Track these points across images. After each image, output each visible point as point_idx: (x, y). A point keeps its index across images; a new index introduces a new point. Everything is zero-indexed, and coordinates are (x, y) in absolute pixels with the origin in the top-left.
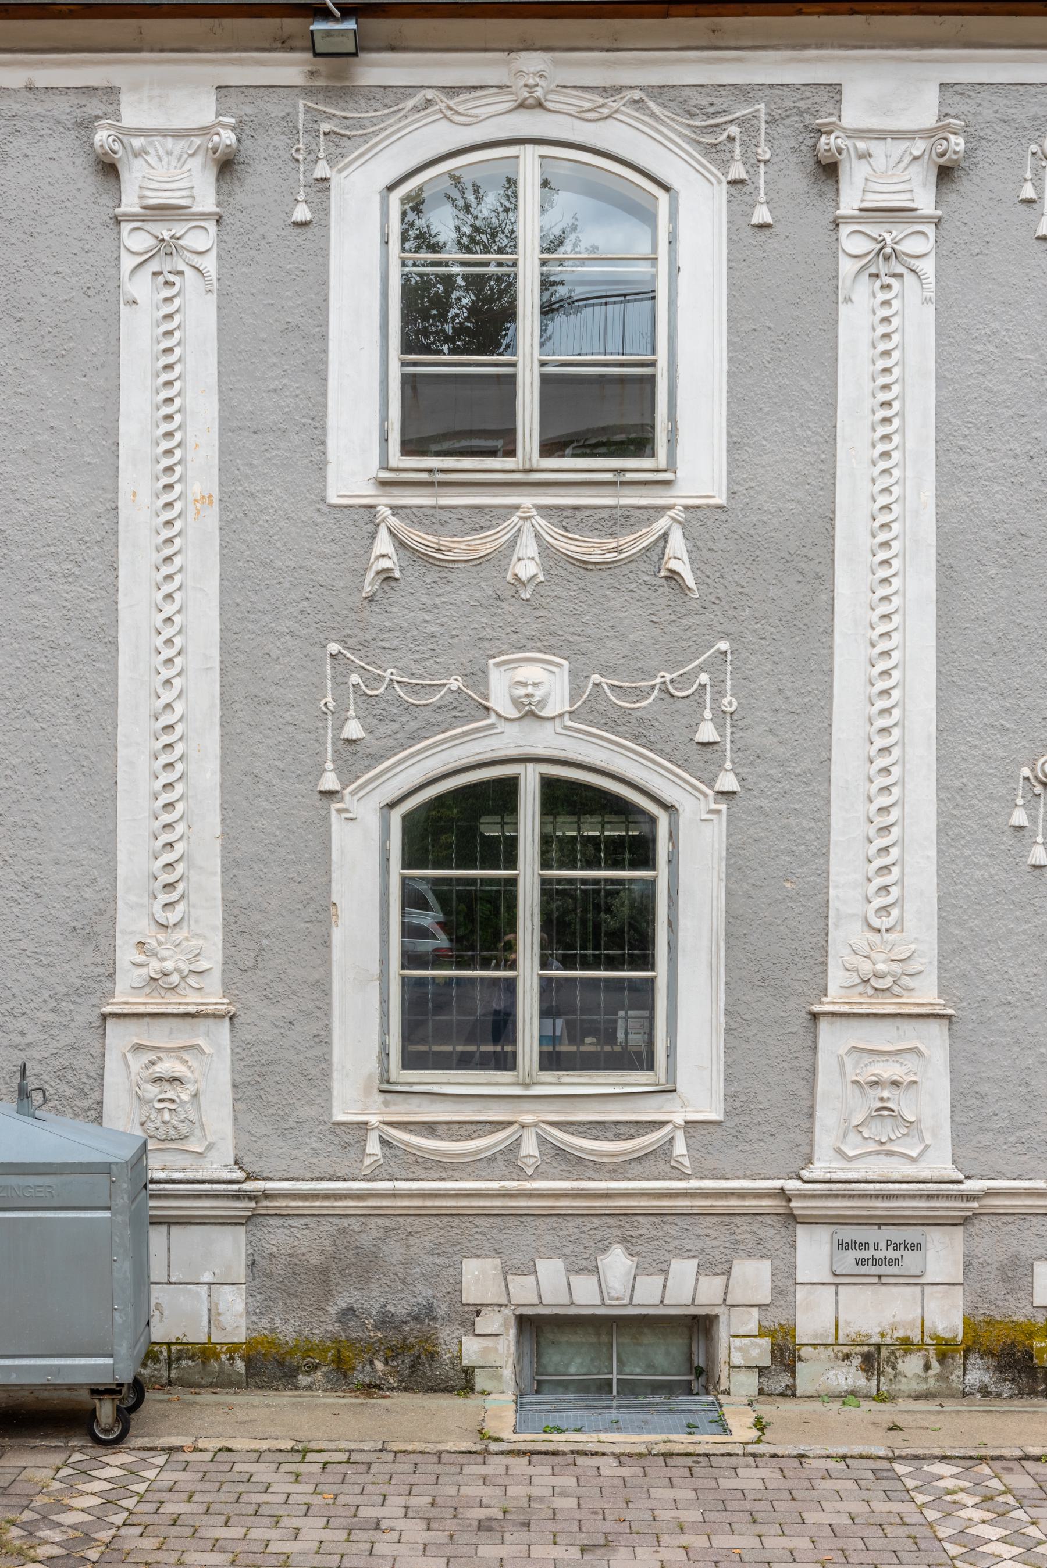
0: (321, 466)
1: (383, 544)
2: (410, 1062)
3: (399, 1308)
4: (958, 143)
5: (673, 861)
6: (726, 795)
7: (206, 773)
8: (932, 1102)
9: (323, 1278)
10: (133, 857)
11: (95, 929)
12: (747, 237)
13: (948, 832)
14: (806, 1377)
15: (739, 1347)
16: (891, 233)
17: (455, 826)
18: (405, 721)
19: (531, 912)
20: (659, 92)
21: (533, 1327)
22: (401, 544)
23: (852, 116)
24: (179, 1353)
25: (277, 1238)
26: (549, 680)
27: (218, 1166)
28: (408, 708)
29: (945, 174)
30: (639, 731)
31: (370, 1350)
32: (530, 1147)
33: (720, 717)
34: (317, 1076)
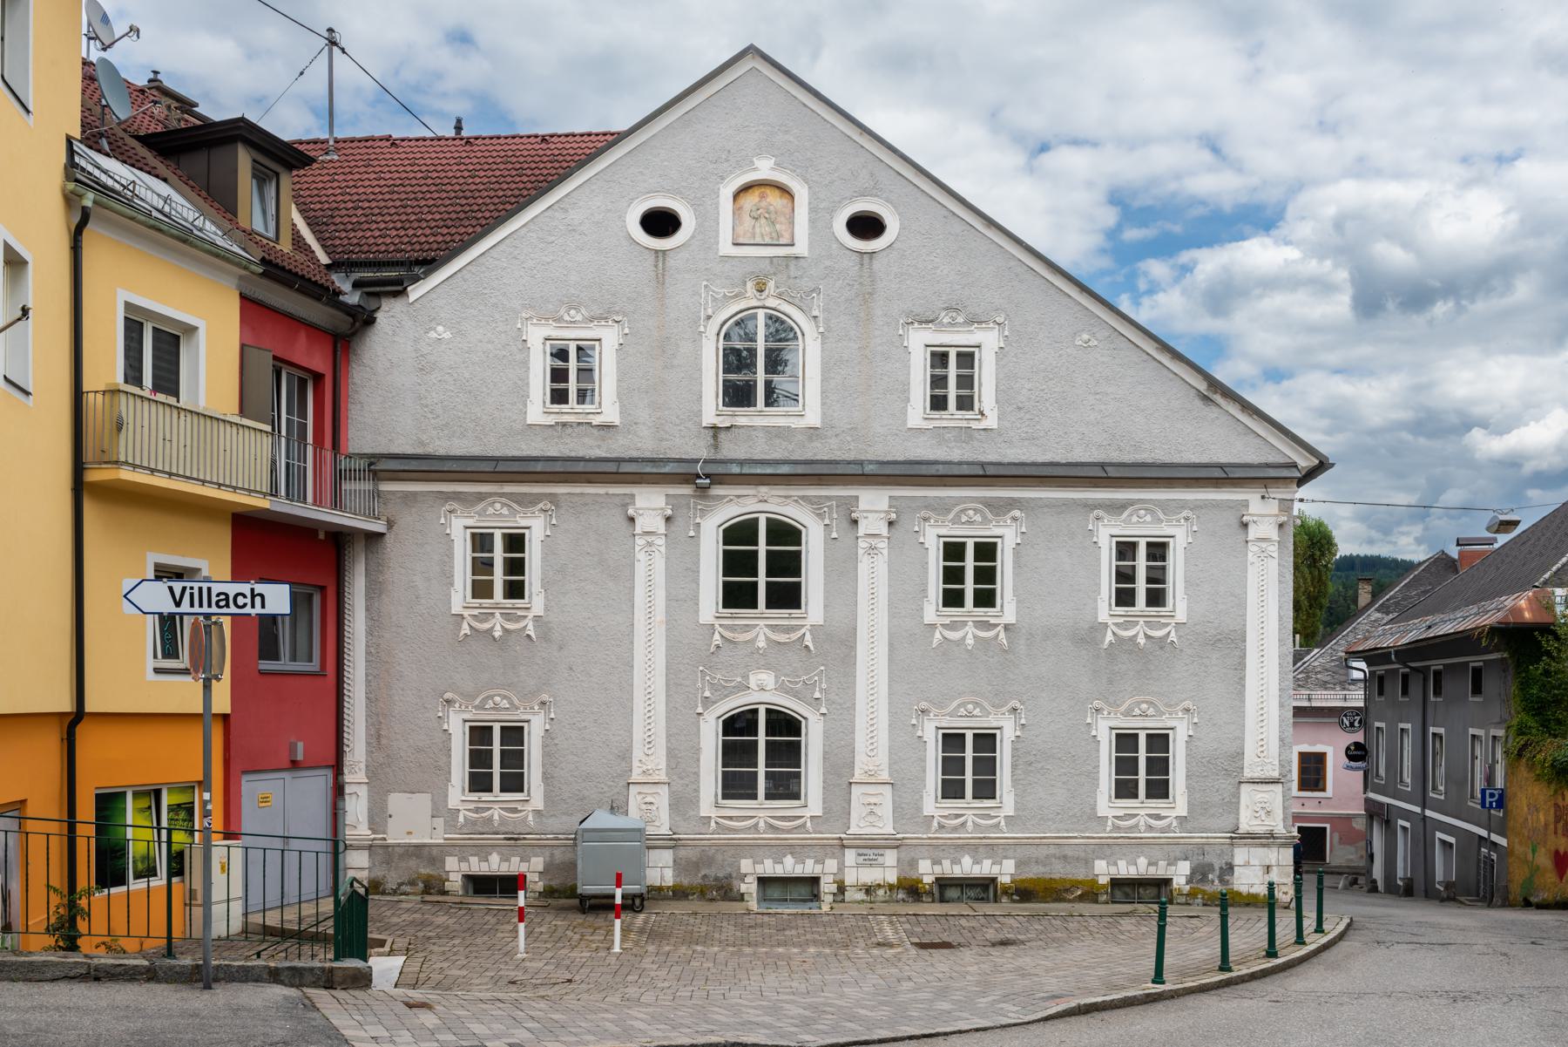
0: (697, 612)
1: (717, 636)
2: (725, 797)
3: (721, 875)
8: (886, 810)
9: (696, 865)
10: (638, 734)
11: (625, 756)
12: (830, 541)
14: (848, 895)
15: (827, 887)
16: (873, 541)
18: (723, 691)
19: (761, 748)
20: (802, 498)
21: (763, 881)
23: (862, 505)
24: (651, 889)
25: (682, 853)
26: (767, 678)
27: (665, 830)
29: (891, 523)
30: (796, 695)
31: (712, 888)
32: (762, 824)
33: (821, 690)
34: (695, 802)
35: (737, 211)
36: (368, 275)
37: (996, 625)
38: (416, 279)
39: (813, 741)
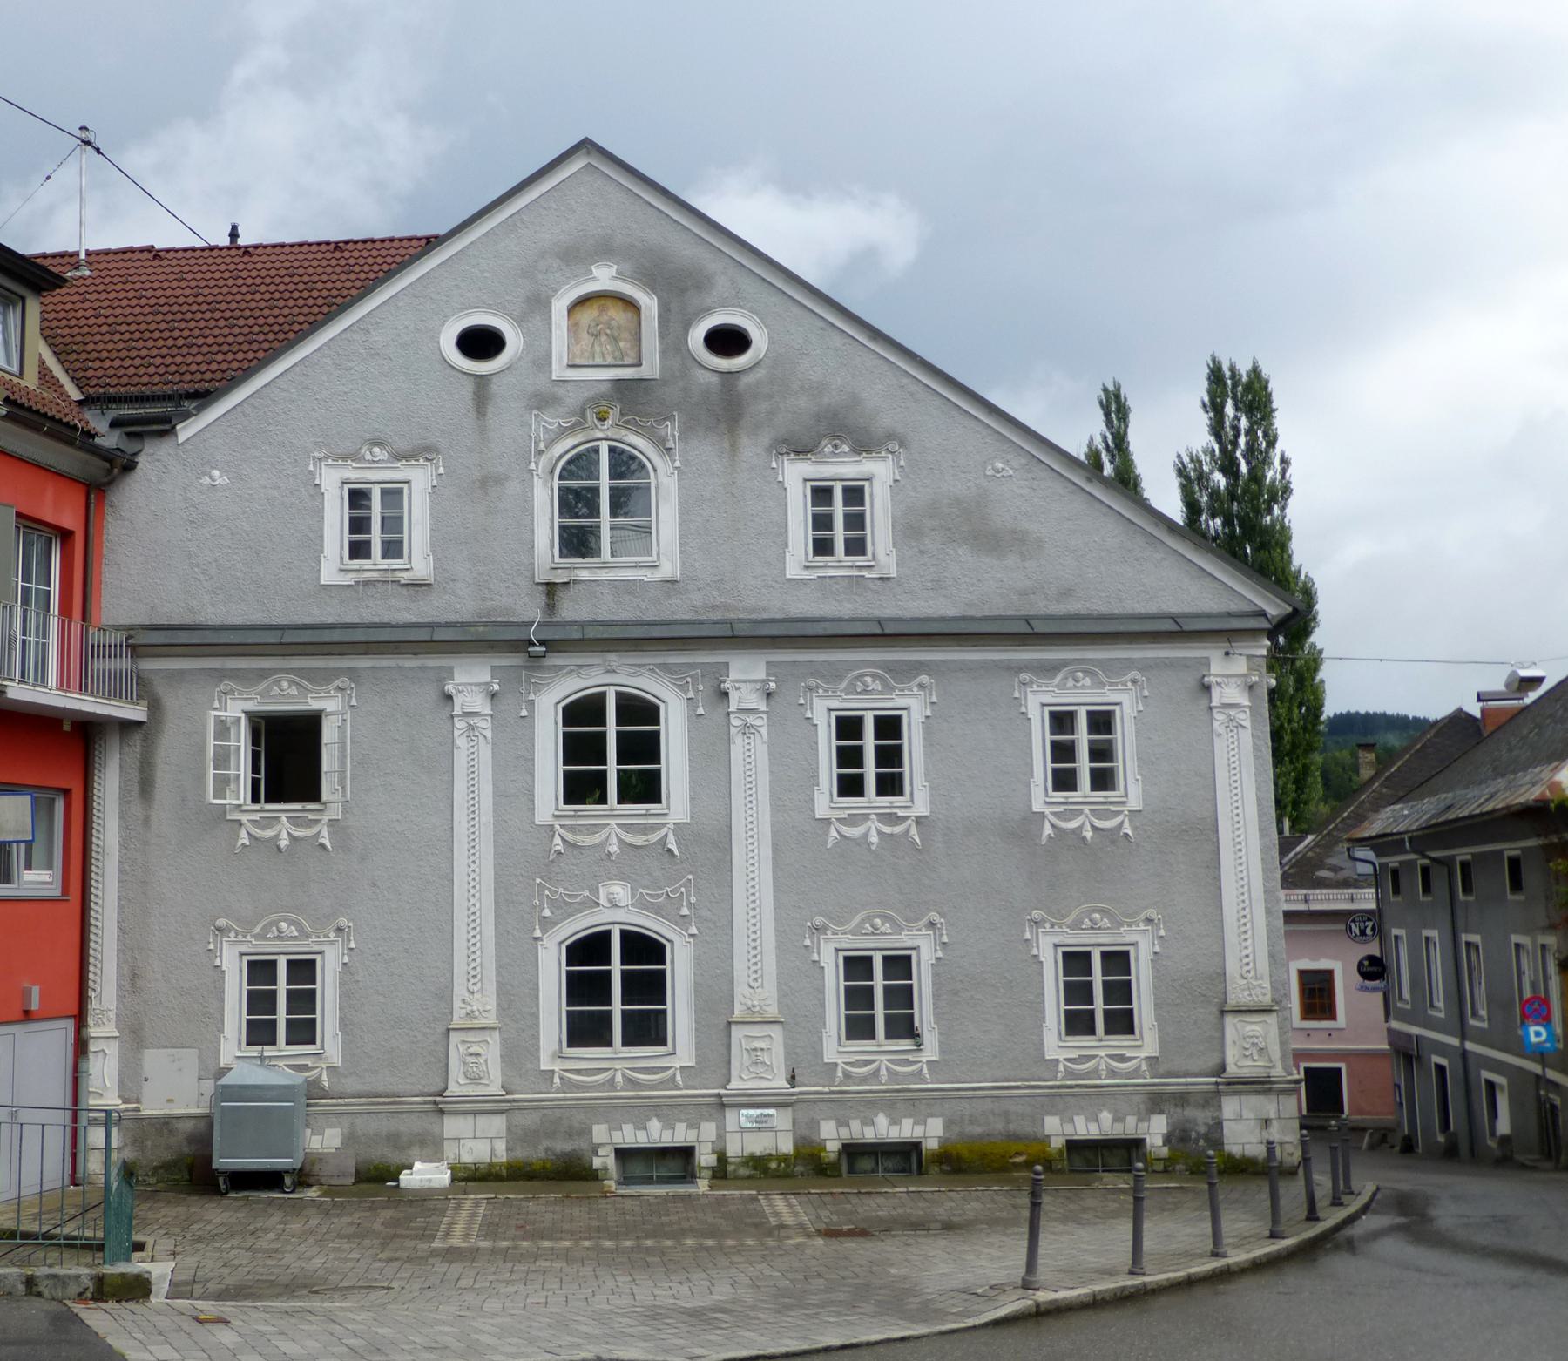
1: (557, 840)
4: (773, 685)
5: (673, 962)
6: (692, 936)
7: (489, 930)
12: (694, 719)
13: (779, 946)
15: (705, 1158)
16: (750, 719)
17: (589, 949)
18: (566, 909)
19: (616, 984)
20: (659, 666)
21: (623, 1154)
22: (563, 839)
23: (733, 676)
26: (621, 891)
28: (567, 904)
30: (657, 910)
32: (619, 1078)
33: (689, 904)
35: (574, 329)
36: (127, 411)
37: (907, 818)
38: (186, 416)
39: (681, 971)
